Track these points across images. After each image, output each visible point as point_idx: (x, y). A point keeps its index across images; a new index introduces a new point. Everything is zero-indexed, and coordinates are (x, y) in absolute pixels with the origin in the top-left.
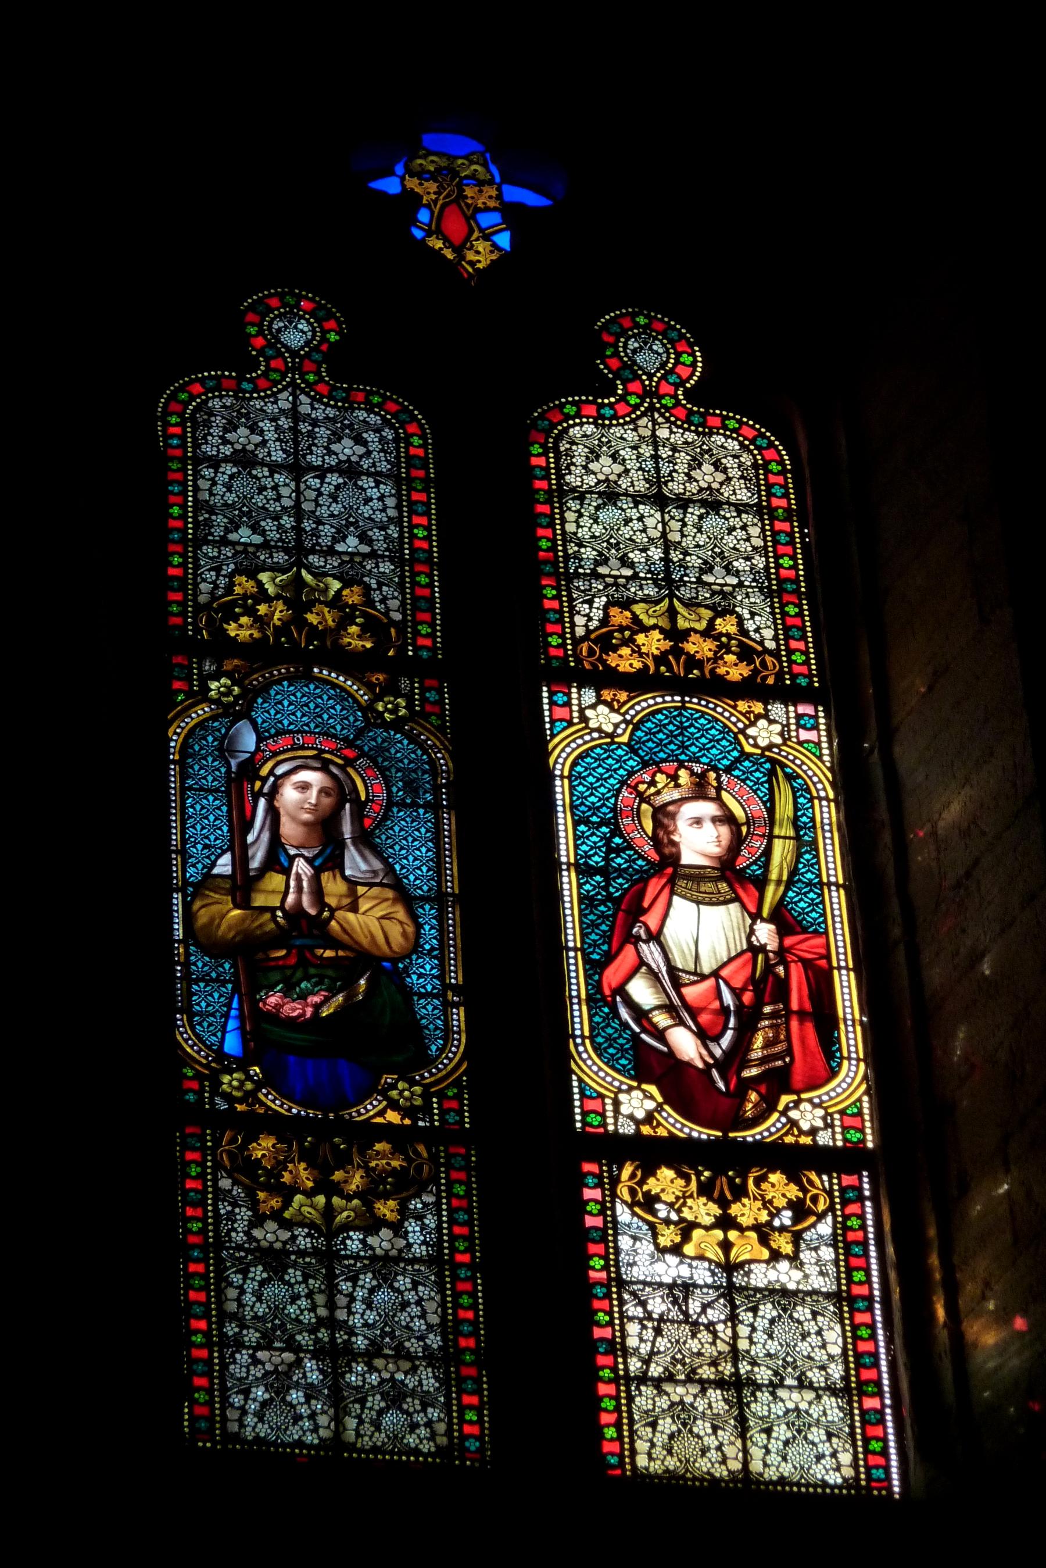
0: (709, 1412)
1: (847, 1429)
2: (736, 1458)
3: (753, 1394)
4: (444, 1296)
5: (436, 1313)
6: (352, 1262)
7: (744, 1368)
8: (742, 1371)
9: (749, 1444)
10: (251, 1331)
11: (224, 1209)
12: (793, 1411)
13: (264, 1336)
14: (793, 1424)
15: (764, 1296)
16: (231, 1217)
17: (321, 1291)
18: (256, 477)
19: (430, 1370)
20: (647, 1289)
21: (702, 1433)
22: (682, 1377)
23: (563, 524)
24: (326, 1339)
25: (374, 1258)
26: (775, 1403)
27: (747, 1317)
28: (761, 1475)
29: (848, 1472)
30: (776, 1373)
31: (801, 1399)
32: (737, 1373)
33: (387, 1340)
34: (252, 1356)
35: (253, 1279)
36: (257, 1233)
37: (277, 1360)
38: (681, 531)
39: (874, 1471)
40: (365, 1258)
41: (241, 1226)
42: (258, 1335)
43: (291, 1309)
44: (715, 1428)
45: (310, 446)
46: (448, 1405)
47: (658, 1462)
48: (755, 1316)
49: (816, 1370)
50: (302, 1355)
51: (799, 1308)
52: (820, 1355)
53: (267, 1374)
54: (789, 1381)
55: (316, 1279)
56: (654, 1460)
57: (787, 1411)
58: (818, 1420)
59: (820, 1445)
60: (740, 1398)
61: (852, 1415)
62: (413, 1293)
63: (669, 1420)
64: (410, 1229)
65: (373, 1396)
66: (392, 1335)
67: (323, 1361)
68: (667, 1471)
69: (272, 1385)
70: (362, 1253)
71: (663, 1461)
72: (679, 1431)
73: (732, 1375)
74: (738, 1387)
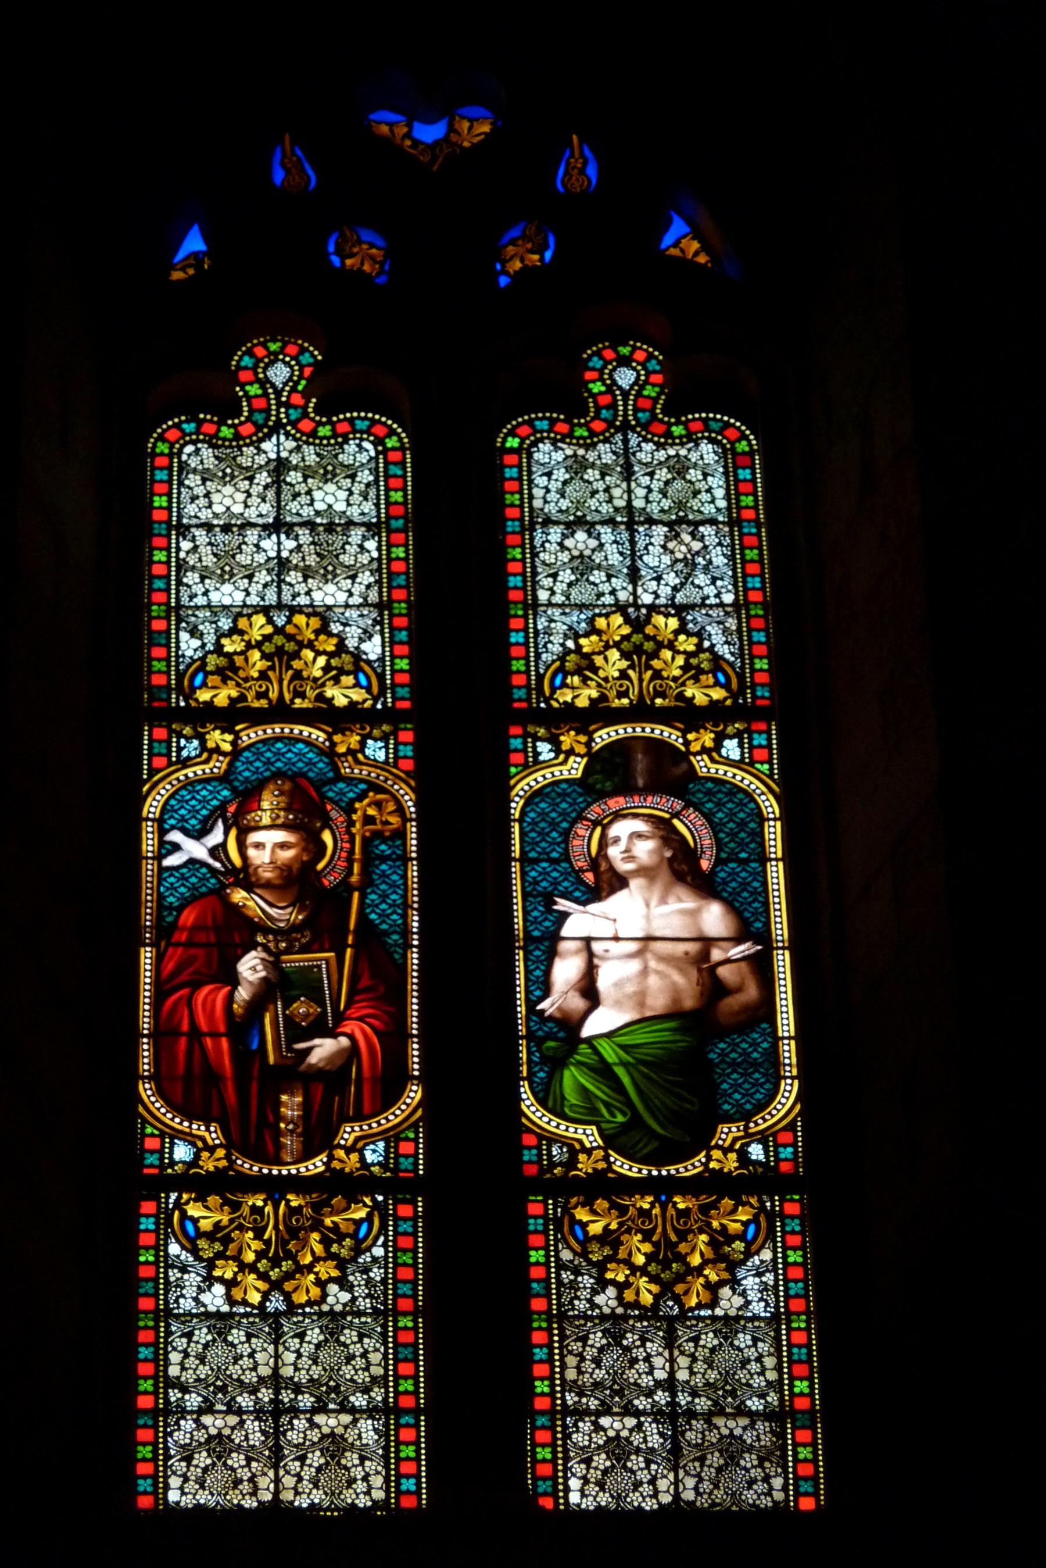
2: (268, 1489)
5: (663, 1368)
6: (582, 1322)
10: (307, 1396)
13: (319, 1399)
15: (595, 1325)
16: (574, 1286)
17: (770, 1354)
20: (307, 1321)
24: (776, 1403)
25: (208, 1315)
26: (710, 1431)
28: (292, 1503)
29: (779, 1496)
31: (737, 1426)
34: (595, 1423)
36: (206, 1298)
37: (219, 1423)
38: (544, 498)
39: (811, 1490)
41: (190, 1292)
43: (741, 1374)
46: (386, 1457)
47: (591, 1499)
49: (755, 1399)
50: (642, 1419)
51: (234, 1331)
52: (758, 1382)
53: (210, 1438)
55: (370, 1338)
56: (587, 1496)
63: (204, 1454)
66: (336, 1389)
67: (265, 1421)
68: (714, 1504)
69: (328, 1450)
70: (194, 1311)
73: (668, 1404)
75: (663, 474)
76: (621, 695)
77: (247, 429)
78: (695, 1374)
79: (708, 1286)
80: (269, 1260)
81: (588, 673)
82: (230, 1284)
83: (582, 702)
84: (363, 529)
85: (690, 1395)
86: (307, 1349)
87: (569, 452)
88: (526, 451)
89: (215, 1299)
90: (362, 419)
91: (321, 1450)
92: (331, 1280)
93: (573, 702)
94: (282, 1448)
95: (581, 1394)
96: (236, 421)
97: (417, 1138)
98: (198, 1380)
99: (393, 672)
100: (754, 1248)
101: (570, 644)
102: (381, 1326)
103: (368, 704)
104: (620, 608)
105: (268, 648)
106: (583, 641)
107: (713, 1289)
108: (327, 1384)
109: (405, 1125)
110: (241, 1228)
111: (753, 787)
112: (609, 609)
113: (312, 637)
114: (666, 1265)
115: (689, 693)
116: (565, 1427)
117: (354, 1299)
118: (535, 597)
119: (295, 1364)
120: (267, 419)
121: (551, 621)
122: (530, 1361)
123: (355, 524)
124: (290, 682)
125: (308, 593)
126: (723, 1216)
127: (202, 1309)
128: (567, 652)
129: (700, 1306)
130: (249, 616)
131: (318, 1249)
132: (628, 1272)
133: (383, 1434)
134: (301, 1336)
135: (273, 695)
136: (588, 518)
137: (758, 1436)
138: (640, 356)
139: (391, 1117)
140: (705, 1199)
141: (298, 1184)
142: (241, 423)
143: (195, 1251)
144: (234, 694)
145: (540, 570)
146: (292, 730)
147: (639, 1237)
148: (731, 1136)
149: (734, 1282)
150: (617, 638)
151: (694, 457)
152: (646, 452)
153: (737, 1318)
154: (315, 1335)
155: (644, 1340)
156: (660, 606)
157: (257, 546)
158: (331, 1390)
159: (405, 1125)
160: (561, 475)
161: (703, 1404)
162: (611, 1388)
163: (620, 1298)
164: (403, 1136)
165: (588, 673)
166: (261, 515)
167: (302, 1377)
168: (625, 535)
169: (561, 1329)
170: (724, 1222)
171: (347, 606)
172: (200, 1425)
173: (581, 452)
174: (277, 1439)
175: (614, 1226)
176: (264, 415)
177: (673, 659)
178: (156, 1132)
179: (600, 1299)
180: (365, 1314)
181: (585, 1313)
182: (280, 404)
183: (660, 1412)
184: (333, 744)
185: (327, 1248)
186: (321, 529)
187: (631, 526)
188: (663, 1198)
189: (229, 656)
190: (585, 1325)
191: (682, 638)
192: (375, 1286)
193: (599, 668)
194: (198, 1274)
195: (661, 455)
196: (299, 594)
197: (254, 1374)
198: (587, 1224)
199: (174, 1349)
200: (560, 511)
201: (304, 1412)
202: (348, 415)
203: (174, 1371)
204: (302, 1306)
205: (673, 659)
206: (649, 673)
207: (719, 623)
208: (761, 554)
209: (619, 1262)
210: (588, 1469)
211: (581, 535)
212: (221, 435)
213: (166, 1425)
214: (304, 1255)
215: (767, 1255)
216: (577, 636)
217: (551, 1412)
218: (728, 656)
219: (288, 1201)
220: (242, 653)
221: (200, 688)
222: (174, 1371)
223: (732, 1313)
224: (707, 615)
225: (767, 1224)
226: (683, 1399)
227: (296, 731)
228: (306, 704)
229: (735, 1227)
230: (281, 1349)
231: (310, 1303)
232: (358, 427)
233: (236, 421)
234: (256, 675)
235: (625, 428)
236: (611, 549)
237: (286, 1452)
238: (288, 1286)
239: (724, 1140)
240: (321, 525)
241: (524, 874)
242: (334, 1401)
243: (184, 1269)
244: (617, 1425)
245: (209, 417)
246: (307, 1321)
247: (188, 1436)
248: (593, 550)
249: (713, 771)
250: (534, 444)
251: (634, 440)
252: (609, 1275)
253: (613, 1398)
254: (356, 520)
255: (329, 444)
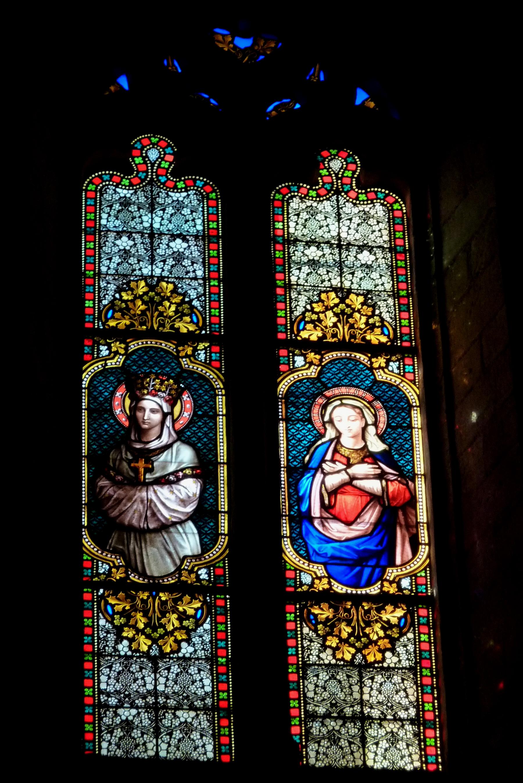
0: (405, 737)
1: (211, 732)
3: (370, 725)
4: (213, 677)
5: (413, 695)
6: (109, 658)
7: (161, 700)
8: (366, 712)
9: (367, 750)
11: (306, 643)
12: (390, 733)
13: (120, 701)
14: (390, 740)
16: (105, 639)
18: (131, 212)
19: (146, 714)
20: (171, 661)
21: (401, 748)
22: (335, 715)
23: (100, 220)
27: (368, 683)
30: (382, 713)
32: (362, 712)
33: (186, 701)
35: (173, 673)
40: (115, 656)
42: (116, 701)
44: (202, 736)
45: (158, 193)
48: (169, 672)
54: (389, 717)
57: (181, 723)
58: (196, 727)
59: (403, 751)
60: (157, 716)
61: (214, 723)
62: (198, 675)
63: (119, 730)
64: (400, 652)
65: (117, 729)
66: (187, 697)
67: (151, 713)
68: (176, 758)
70: (113, 654)
71: (381, 763)
72: (183, 737)
73: (153, 703)
74: (363, 719)
75: (304, 215)
76: (141, 324)
77: (323, 192)
78: (317, 694)
79: (176, 641)
80: (355, 638)
81: (317, 323)
82: (131, 640)
83: (121, 326)
84: (115, 234)
85: (165, 698)
86: (172, 676)
87: (309, 204)
88: (285, 203)
89: (327, 657)
90: (382, 192)
91: (180, 730)
92: (183, 640)
93: (309, 338)
94: (160, 728)
95: (371, 708)
96: (317, 187)
97: (225, 566)
98: (174, 692)
99: (210, 316)
100: (200, 622)
101: (308, 307)
102: (210, 665)
103: (198, 332)
104: (335, 290)
105: (337, 310)
106: (314, 305)
107: (178, 642)
108: (386, 705)
109: (219, 560)
110: (136, 611)
111: (211, 377)
112: (138, 278)
113: (360, 307)
114: (358, 638)
115: (368, 338)
116: (100, 714)
117: (195, 651)
118: (290, 280)
119: (107, 682)
120: (332, 187)
121: (108, 283)
122: (83, 677)
123: (111, 231)
124: (349, 329)
125: (329, 280)
126: (185, 605)
127: (117, 653)
128: (307, 310)
129: (172, 652)
130: (137, 281)
131: (177, 624)
132: (134, 632)
133: (212, 722)
134: (168, 669)
135: (340, 336)
136: (317, 240)
137: (141, 720)
138: (164, 144)
139: (211, 555)
140: (176, 596)
141: (368, 598)
142: (319, 188)
143: (316, 631)
144: (128, 322)
145: (102, 256)
146: (351, 355)
147: (141, 614)
148: (192, 564)
149: (393, 650)
150: (141, 293)
151: (372, 212)
152: (348, 208)
153: (190, 659)
154: (175, 669)
155: (141, 668)
156: (165, 277)
157: (168, 245)
158: (126, 696)
159: (219, 560)
160: (356, 220)
161: (172, 702)
162: (386, 705)
163: (130, 647)
164: (217, 565)
165: (317, 323)
166: (115, 227)
167: (111, 689)
168: (148, 241)
169: (99, 662)
170: (185, 608)
171: (107, 274)
172: (323, 725)
173: (315, 204)
174: (157, 723)
175: (127, 608)
176: (330, 185)
177: (360, 318)
178: (89, 558)
179: (120, 647)
180: (201, 659)
181: (111, 654)
182: (338, 178)
183: (208, 709)
184: (372, 363)
185: (181, 623)
186: (147, 235)
187: (152, 236)
188: (154, 593)
189: (126, 302)
190: (169, 661)
191: (365, 307)
192: (410, 654)
193: (322, 321)
194: (318, 643)
195: (303, 206)
196: (378, 285)
197: (202, 690)
198: (317, 615)
199: (103, 674)
200: (355, 240)
201: (112, 707)
202: (287, 184)
203: (103, 686)
204: (169, 654)
205: (170, 307)
206: (156, 314)
207: (195, 289)
208: (218, 253)
209: (130, 627)
210: (170, 738)
211: (366, 253)
212: (310, 195)
213: (100, 714)
214: (169, 626)
215: (410, 635)
216: (312, 302)
217: (94, 706)
218: (199, 308)
219: (160, 597)
220: (132, 301)
221: (111, 318)
222: (103, 686)
223: (188, 655)
224: (189, 285)
225: (209, 609)
226: (161, 700)
227: (353, 355)
228: (166, 330)
229: (190, 612)
230: (158, 676)
231: (376, 662)
232: (379, 196)
233: (317, 187)
234: (139, 312)
235: (338, 192)
236: (381, 261)
237: (162, 730)
238: (160, 642)
239: (188, 566)
240: (146, 233)
241: (287, 430)
242: (127, 702)
243: (311, 641)
244: (186, 715)
245: (115, 173)
246: (171, 661)
247: (170, 722)
248: (131, 247)
249: (191, 367)
250: (292, 197)
251: (342, 201)
252: (125, 634)
253: (125, 698)
254: (299, 238)
255: (363, 204)
